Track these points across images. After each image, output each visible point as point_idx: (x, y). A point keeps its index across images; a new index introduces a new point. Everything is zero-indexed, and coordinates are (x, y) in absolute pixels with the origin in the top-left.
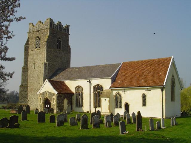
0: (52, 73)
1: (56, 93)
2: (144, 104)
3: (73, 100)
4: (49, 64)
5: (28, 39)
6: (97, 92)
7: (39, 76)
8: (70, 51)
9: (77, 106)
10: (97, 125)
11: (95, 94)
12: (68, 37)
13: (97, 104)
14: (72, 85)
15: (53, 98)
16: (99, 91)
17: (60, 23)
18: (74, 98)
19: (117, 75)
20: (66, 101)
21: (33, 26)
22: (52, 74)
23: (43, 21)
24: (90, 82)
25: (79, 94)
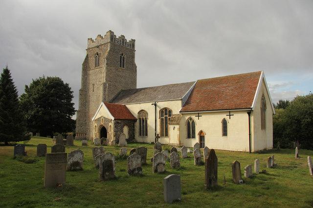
0: (113, 96)
1: (113, 118)
2: (225, 133)
3: (135, 127)
4: (110, 85)
5: (87, 56)
6: (164, 118)
7: (98, 101)
8: (136, 70)
9: (140, 135)
10: (137, 172)
11: (162, 120)
13: (165, 133)
14: (134, 108)
16: (167, 116)
17: (123, 36)
18: (137, 124)
19: (190, 96)
20: (126, 130)
21: (91, 42)
22: (113, 97)
23: (103, 35)
24: (155, 105)
25: (143, 120)
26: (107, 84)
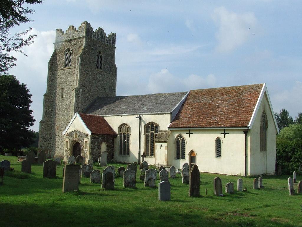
12: (114, 52)
15: (85, 141)
17: (101, 29)
26: (81, 90)
